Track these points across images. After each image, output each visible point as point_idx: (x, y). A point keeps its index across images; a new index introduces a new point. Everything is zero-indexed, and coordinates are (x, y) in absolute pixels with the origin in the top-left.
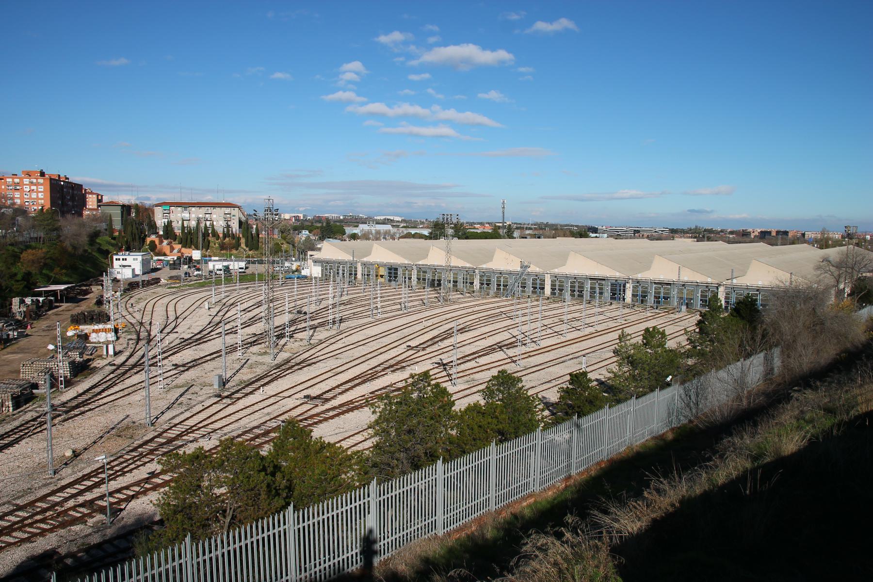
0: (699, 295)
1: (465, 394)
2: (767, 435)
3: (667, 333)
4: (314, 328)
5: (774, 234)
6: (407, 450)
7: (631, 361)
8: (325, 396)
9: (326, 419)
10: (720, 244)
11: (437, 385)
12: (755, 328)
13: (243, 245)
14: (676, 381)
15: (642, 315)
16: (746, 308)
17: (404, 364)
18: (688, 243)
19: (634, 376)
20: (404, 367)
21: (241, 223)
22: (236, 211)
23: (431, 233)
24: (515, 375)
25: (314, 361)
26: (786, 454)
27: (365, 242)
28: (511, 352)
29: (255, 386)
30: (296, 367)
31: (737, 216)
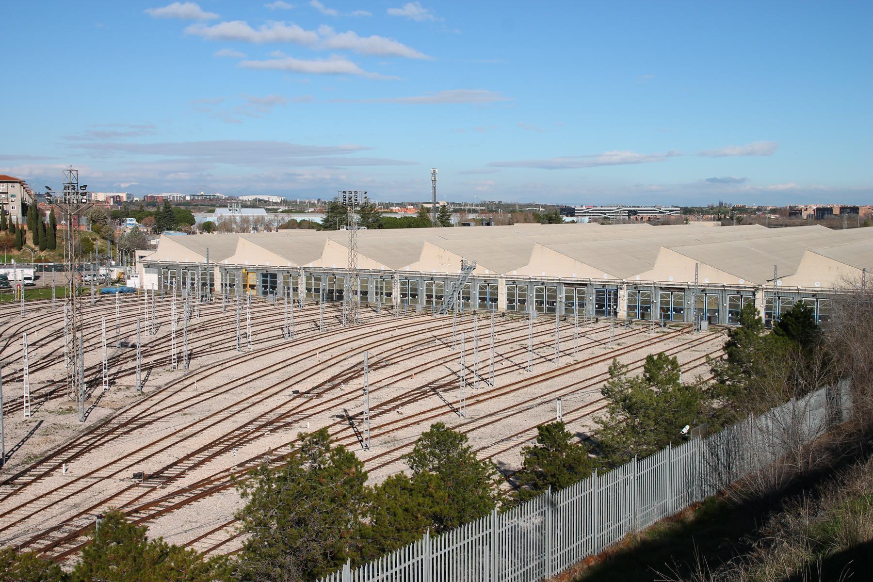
0: (727, 304)
1: (383, 463)
2: (834, 511)
3: (680, 362)
4: (148, 368)
5: (836, 211)
6: (295, 551)
7: (630, 406)
8: (166, 474)
9: (169, 510)
10: (756, 229)
11: (340, 449)
12: (811, 352)
13: (30, 243)
14: (696, 434)
15: (644, 336)
16: (798, 323)
17: (289, 420)
18: (708, 227)
19: (633, 427)
20: (289, 424)
21: (25, 207)
22: (16, 189)
23: (326, 221)
24: (457, 430)
25: (148, 419)
26: (866, 539)
27: (226, 235)
28: (450, 396)
29: (53, 463)
30: (121, 431)
31: (781, 187)
